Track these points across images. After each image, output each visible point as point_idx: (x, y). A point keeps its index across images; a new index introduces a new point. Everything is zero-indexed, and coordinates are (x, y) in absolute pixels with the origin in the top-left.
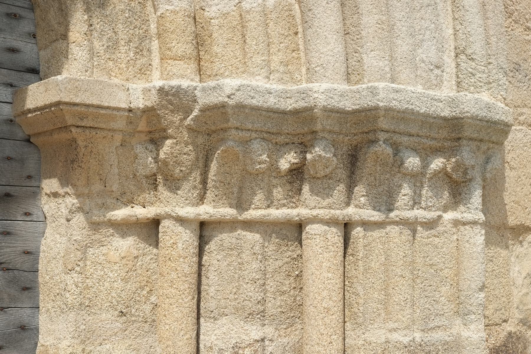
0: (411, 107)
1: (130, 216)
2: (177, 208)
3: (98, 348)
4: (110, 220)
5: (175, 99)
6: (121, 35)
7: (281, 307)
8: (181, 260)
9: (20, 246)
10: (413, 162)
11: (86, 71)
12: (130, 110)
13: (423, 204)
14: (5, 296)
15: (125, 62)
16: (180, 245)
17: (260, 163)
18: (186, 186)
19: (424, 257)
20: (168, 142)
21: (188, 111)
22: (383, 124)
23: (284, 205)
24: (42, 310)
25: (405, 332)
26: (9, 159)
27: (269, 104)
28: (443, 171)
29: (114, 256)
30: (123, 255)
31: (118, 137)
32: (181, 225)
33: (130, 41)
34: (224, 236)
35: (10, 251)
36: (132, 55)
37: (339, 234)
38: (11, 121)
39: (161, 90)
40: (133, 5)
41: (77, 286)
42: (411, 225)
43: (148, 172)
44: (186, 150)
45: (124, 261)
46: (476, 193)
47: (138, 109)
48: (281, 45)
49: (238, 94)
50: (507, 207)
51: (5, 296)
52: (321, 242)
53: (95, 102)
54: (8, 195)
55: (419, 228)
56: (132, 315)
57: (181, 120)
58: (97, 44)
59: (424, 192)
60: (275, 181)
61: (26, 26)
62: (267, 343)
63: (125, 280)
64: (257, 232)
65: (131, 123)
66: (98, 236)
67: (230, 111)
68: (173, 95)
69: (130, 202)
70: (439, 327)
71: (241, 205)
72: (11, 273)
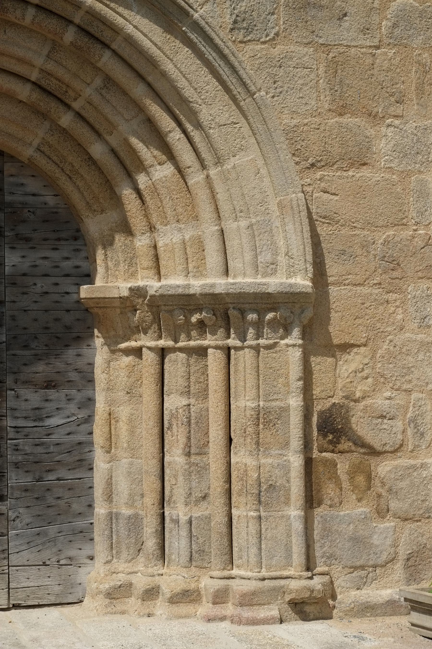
0: (243, 291)
1: (129, 346)
2: (147, 342)
3: (117, 409)
4: (119, 349)
5: (138, 292)
6: (120, 259)
7: (199, 389)
8: (150, 367)
9: (86, 361)
10: (252, 317)
11: (104, 278)
12: (120, 298)
13: (265, 337)
14: (80, 385)
15: (123, 271)
16: (149, 360)
17: (179, 320)
18: (150, 332)
19: (265, 364)
20: (138, 312)
21: (145, 297)
22: (228, 300)
23: (198, 339)
24: (96, 391)
25: (252, 402)
26: (78, 320)
27: (178, 292)
28: (275, 318)
29: (123, 365)
30: (127, 365)
31: (118, 311)
32: (150, 350)
33: (125, 261)
34: (172, 355)
35: (80, 363)
36: (127, 267)
37: (222, 353)
38: (78, 301)
39: (130, 289)
40: (126, 242)
41: (106, 380)
42: (257, 349)
43: (135, 325)
44: (147, 315)
45: (127, 368)
46: (295, 330)
47: (125, 296)
48: (194, 258)
49: (160, 290)
50: (332, 334)
51: (80, 385)
52: (214, 359)
53: (102, 296)
54: (78, 337)
55: (262, 349)
56: (133, 394)
57: (143, 301)
58: (110, 264)
59: (265, 330)
60: (191, 328)
61: (83, 254)
62: (191, 407)
63: (129, 377)
64: (184, 353)
65: (122, 303)
66: (115, 356)
67: (158, 298)
68: (137, 290)
69: (128, 339)
70: (277, 399)
71: (176, 341)
72: (82, 374)
